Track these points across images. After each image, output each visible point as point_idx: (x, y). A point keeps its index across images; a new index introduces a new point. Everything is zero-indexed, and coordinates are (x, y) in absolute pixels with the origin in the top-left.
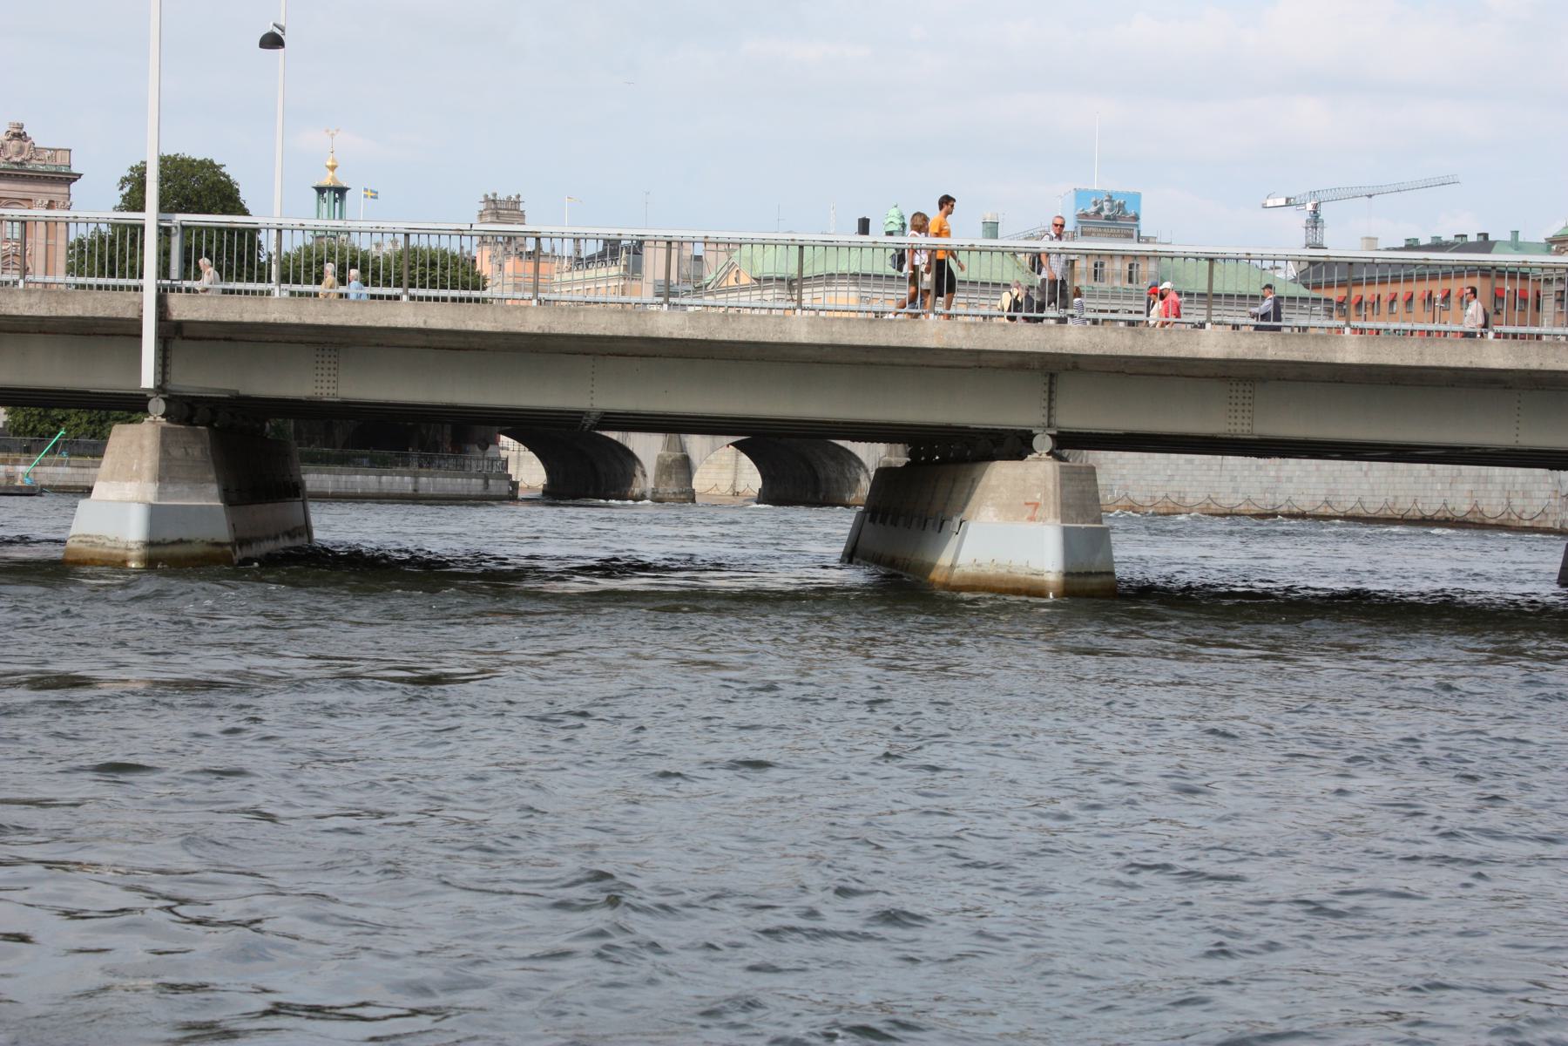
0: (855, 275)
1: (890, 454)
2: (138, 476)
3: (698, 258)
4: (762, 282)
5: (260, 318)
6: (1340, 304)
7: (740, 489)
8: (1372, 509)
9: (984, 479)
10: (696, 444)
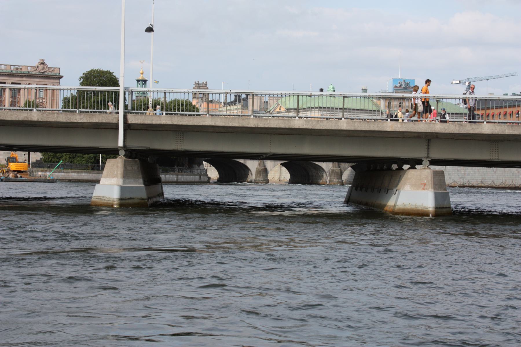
0: (320, 108)
1: (333, 167)
2: (116, 176)
3: (267, 102)
4: (288, 110)
5: (159, 122)
6: (482, 115)
7: (282, 179)
8: (497, 184)
9: (405, 175)
10: (269, 164)
